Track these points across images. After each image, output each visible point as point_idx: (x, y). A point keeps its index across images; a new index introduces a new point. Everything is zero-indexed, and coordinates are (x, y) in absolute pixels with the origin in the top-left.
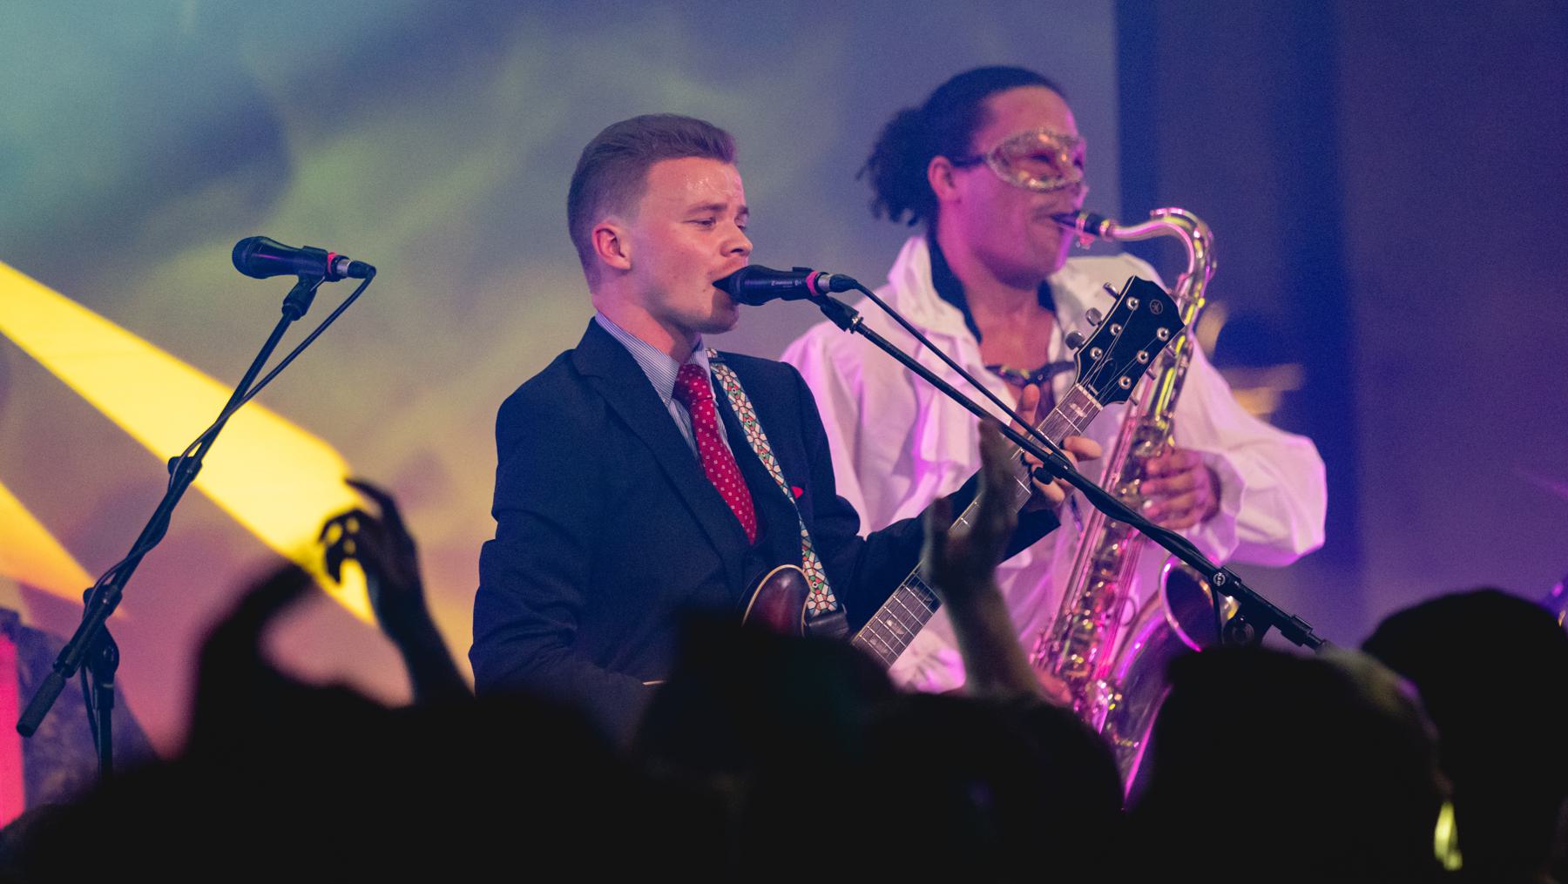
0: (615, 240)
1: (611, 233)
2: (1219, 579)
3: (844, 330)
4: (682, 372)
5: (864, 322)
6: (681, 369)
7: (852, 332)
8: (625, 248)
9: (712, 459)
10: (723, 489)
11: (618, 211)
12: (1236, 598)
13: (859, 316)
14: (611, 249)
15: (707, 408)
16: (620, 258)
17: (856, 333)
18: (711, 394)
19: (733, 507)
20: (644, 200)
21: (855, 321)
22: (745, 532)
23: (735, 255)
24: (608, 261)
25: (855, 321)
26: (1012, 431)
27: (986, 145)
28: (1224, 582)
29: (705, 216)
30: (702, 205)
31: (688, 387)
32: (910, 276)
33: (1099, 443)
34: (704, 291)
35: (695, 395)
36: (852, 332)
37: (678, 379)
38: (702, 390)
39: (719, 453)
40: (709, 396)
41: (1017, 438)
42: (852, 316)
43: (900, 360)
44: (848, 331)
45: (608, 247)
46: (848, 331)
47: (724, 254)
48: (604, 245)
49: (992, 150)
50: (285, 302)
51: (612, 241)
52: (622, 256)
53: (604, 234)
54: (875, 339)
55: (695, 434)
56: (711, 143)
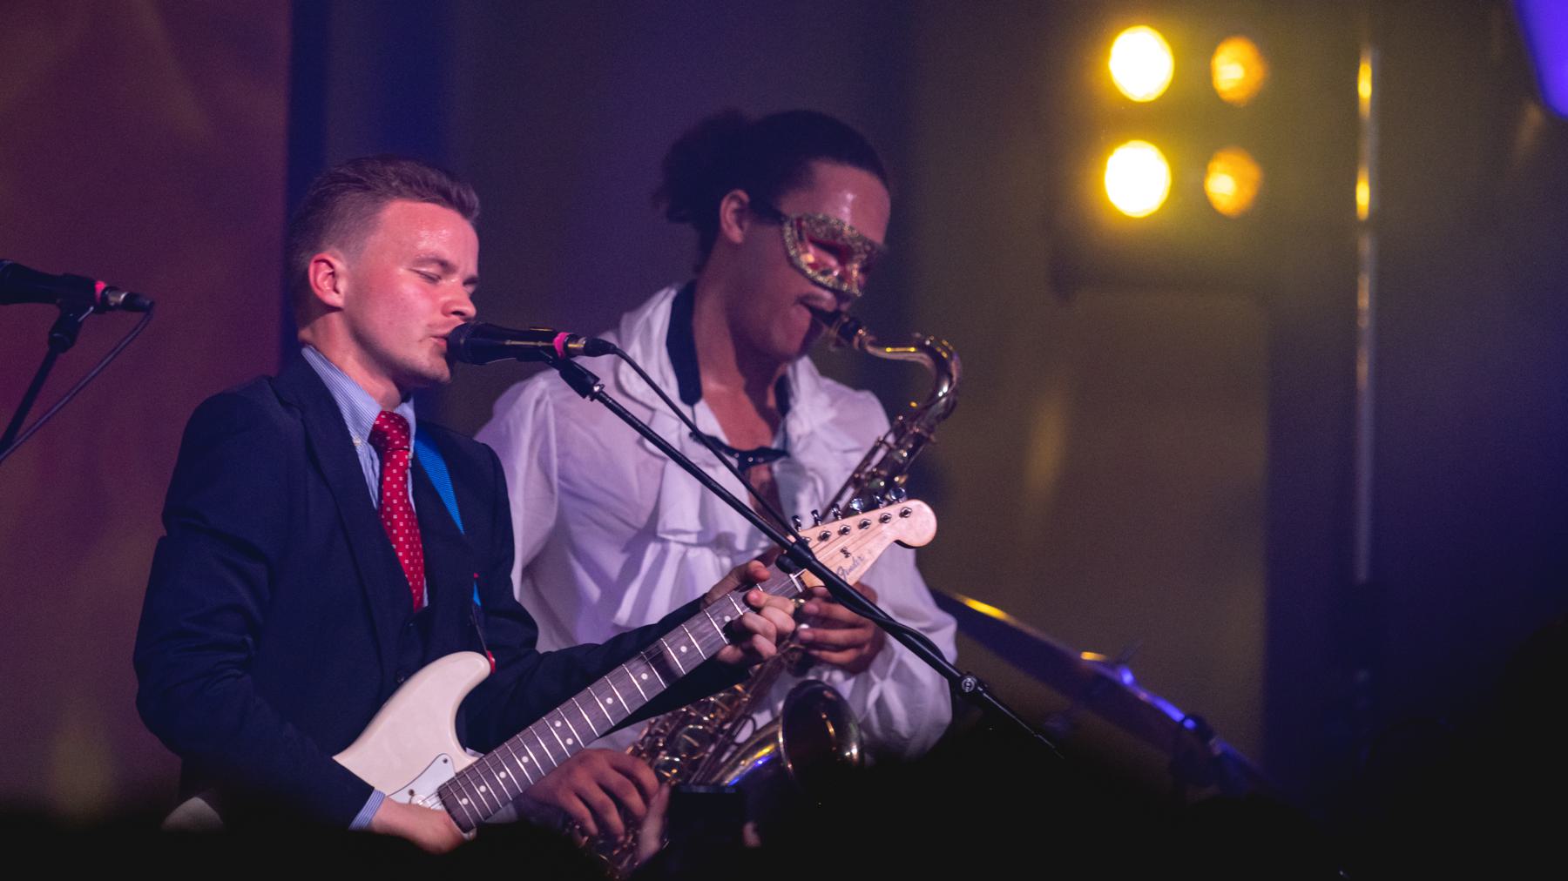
0: (333, 274)
1: (330, 265)
2: (968, 684)
3: (584, 397)
4: (383, 417)
5: (605, 390)
6: (382, 413)
7: (592, 400)
8: (342, 285)
9: (392, 513)
10: (389, 524)
11: (341, 246)
12: (963, 691)
13: (600, 382)
14: (326, 283)
15: (401, 458)
16: (335, 294)
17: (596, 400)
18: (409, 446)
19: (401, 554)
20: (372, 238)
21: (596, 389)
22: (411, 592)
23: (454, 317)
24: (318, 292)
25: (596, 389)
26: (648, 428)
27: (791, 205)
28: (972, 689)
29: (432, 269)
30: (431, 256)
31: (386, 433)
32: (648, 327)
33: (613, 353)
34: (421, 341)
35: (391, 442)
36: (592, 400)
37: (378, 422)
38: (401, 440)
39: (401, 494)
40: (406, 447)
41: (672, 453)
42: (595, 384)
43: (910, 649)
44: (588, 398)
45: (324, 279)
46: (588, 398)
47: (445, 313)
48: (320, 277)
49: (794, 216)
50: (50, 333)
51: (330, 274)
52: (336, 291)
53: (324, 264)
54: (667, 449)
55: (381, 480)
56: (454, 194)
